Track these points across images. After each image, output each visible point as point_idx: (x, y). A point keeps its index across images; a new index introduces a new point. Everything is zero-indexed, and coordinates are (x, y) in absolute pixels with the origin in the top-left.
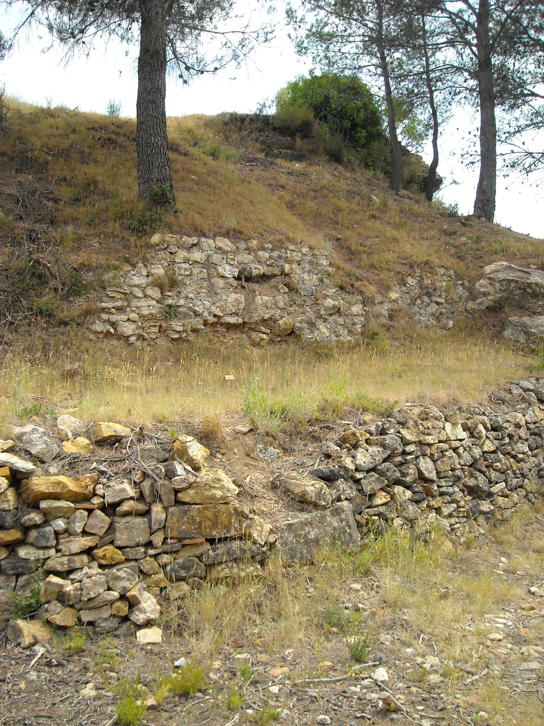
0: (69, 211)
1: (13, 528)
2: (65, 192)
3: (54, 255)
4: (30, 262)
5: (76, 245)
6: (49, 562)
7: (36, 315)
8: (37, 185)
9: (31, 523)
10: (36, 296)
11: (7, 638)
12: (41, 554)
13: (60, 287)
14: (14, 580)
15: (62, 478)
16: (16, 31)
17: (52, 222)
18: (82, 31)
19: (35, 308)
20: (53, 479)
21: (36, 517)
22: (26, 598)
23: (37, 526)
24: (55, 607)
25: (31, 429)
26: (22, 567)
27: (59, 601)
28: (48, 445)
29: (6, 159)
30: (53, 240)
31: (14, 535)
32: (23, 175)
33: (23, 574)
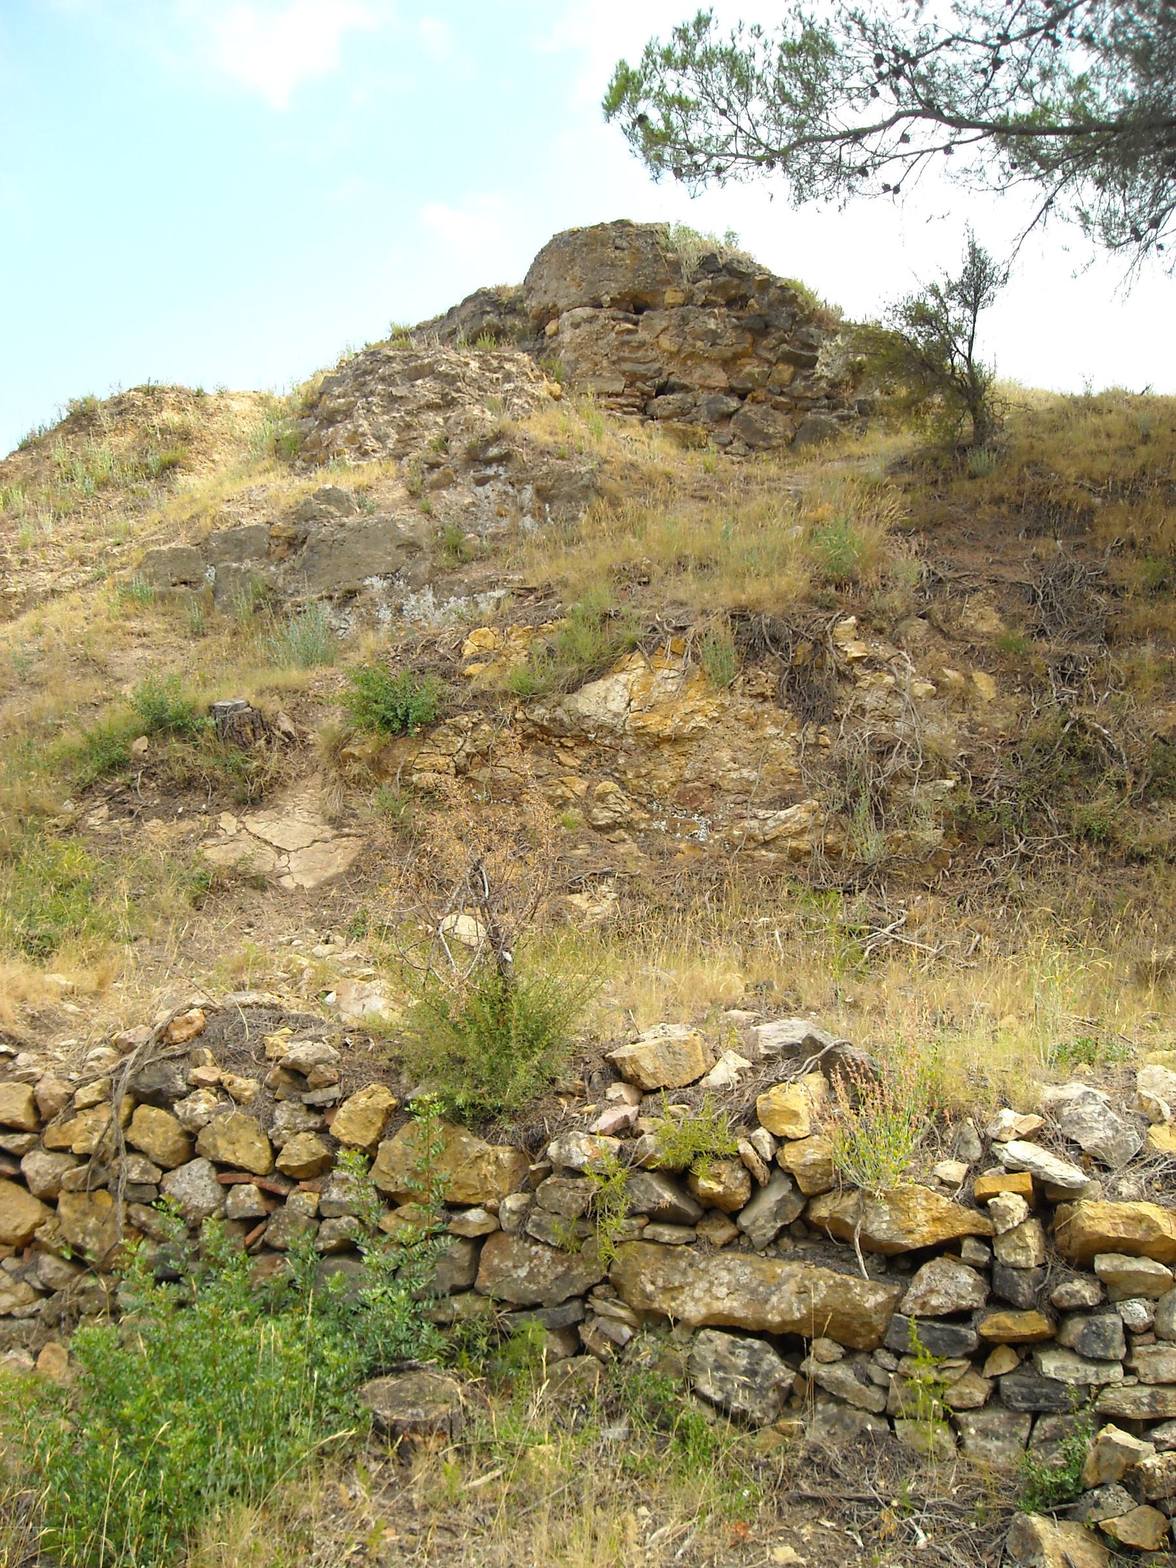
0: (1145, 612)
1: (1032, 1307)
2: (1134, 572)
3: (1114, 710)
4: (1064, 726)
5: (1164, 686)
6: (1107, 1393)
7: (1079, 840)
8: (1073, 560)
9: (1074, 1302)
10: (1078, 798)
11: (1005, 1551)
12: (1090, 1373)
13: (1129, 778)
14: (1028, 1424)
15: (1146, 1208)
16: (1016, 244)
17: (1108, 639)
18: (1155, 223)
19: (1074, 825)
20: (1127, 1208)
21: (1084, 1290)
22: (1053, 1468)
23: (1085, 1310)
24: (1116, 1498)
25: (1080, 1092)
26: (1047, 1397)
27: (1127, 1487)
28: (1117, 1131)
29: (1004, 509)
30: (1111, 677)
31: (1034, 1324)
32: (1041, 541)
33: (1050, 1413)
